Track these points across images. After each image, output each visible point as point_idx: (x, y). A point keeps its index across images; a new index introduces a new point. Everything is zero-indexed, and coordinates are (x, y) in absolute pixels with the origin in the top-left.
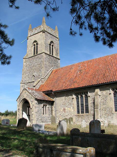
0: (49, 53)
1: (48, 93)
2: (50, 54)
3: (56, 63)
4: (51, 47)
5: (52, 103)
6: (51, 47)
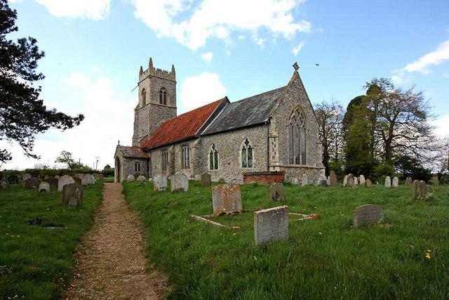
1: (145, 150)
2: (161, 102)
4: (163, 94)
5: (148, 160)
6: (163, 94)
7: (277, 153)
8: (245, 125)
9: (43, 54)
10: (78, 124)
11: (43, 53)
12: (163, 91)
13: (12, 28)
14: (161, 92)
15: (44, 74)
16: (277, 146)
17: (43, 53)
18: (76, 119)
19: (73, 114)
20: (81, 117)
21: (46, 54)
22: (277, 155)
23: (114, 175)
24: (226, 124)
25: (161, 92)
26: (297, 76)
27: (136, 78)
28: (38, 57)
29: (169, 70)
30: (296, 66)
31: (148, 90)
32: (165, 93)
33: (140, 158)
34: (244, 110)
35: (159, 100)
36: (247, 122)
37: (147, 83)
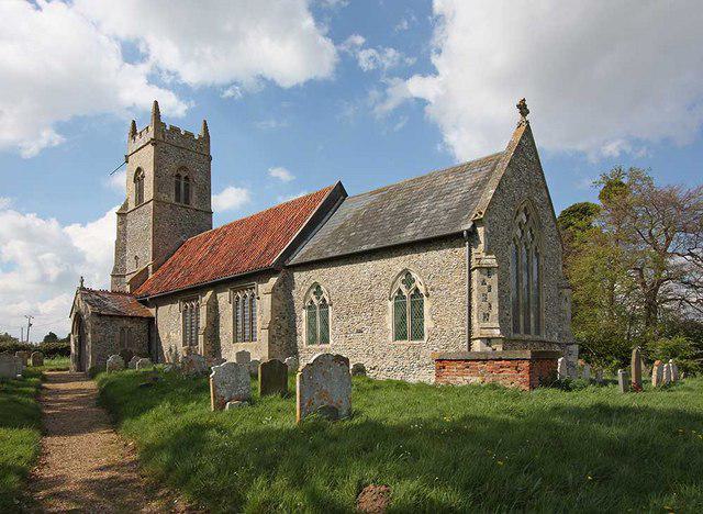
0: (173, 199)
2: (178, 200)
3: (197, 223)
7: (495, 305)
12: (184, 174)
14: (178, 176)
29: (198, 132)
31: (149, 172)
32: (186, 178)
33: (132, 317)
36: (409, 234)
37: (146, 159)
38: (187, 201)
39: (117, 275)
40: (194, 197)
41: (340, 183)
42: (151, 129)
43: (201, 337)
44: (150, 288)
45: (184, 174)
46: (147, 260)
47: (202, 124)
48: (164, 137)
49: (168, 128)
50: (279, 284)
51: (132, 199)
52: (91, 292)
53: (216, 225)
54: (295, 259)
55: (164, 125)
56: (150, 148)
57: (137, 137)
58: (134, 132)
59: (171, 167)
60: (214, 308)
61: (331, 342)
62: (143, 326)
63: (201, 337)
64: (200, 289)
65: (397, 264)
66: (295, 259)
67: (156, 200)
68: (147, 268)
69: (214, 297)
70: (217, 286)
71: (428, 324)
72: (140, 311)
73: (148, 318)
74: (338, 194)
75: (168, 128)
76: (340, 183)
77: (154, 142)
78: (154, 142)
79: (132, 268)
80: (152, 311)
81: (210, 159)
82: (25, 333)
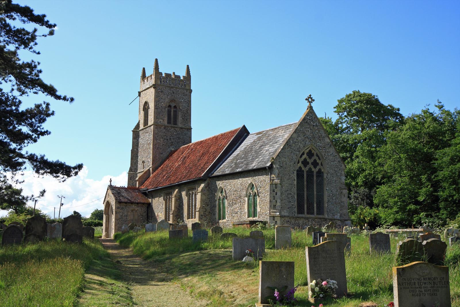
2: (169, 122)
3: (182, 137)
7: (279, 201)
8: (250, 168)
9: (53, 114)
10: (76, 173)
11: (53, 112)
12: (173, 105)
13: (23, 87)
14: (170, 106)
15: (49, 130)
16: (279, 194)
17: (53, 112)
18: (75, 168)
19: (71, 163)
20: (80, 167)
21: (56, 114)
22: (278, 204)
23: (102, 225)
24: (236, 164)
25: (170, 106)
26: (311, 108)
27: (138, 85)
28: (48, 115)
29: (182, 74)
30: (310, 99)
31: (152, 105)
32: (175, 107)
33: (138, 203)
34: (257, 147)
35: (166, 119)
36: (254, 165)
37: (150, 96)
38: (175, 123)
39: (131, 177)
40: (180, 119)
41: (244, 127)
42: (153, 77)
43: (171, 216)
44: (148, 186)
45: (173, 105)
46: (149, 165)
47: (186, 67)
48: (161, 82)
49: (164, 75)
50: (205, 187)
51: (142, 122)
52: (116, 188)
53: (195, 139)
54: (216, 173)
55: (161, 73)
56: (152, 90)
57: (146, 81)
58: (144, 76)
59: (163, 104)
60: (179, 199)
61: (226, 218)
62: (144, 209)
63: (171, 216)
64: (171, 188)
65: (248, 180)
66: (225, 168)
67: (155, 124)
68: (149, 170)
69: (180, 192)
70: (180, 186)
71: (258, 209)
72: (141, 199)
73: (147, 204)
74: (243, 133)
75: (164, 75)
76: (244, 127)
77: (154, 86)
78: (154, 86)
79: (141, 170)
80: (150, 200)
81: (191, 91)
82: (57, 210)
